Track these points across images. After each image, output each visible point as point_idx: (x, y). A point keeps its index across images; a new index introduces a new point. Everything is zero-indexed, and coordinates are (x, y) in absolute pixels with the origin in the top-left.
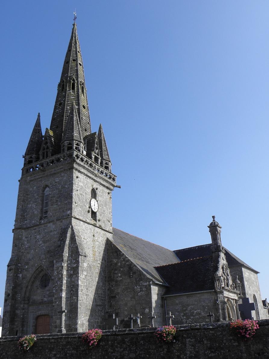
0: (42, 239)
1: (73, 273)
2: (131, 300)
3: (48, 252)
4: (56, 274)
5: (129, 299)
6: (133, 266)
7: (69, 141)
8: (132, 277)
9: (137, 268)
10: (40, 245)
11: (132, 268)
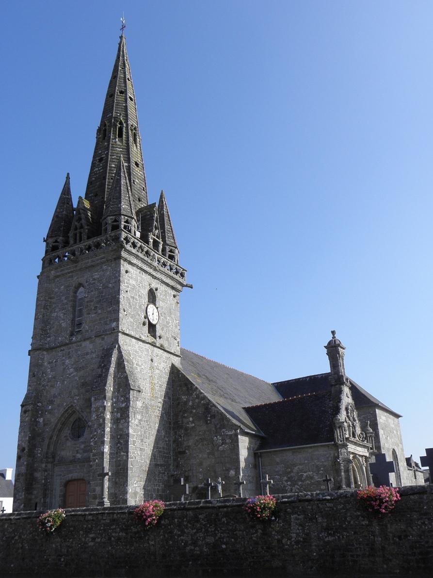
2: (208, 458)
5: (205, 456)
6: (211, 406)
8: (211, 423)
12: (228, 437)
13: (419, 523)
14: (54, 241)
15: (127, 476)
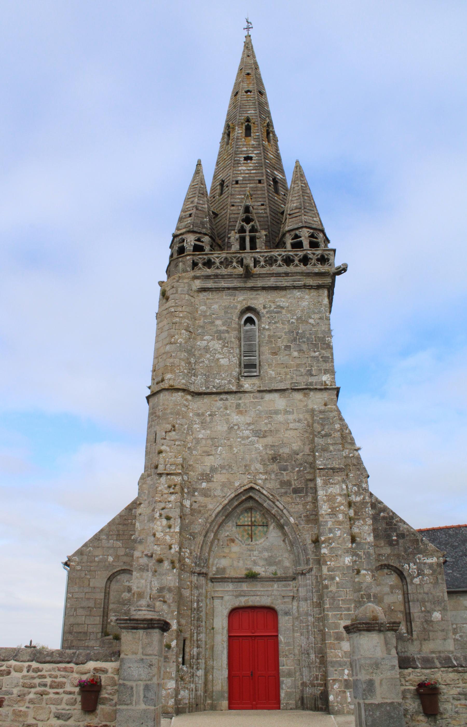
0: (249, 424)
1: (355, 514)
2: (392, 593)
3: (274, 459)
4: (325, 511)
5: (387, 589)
6: (397, 521)
7: (312, 231)
8: (398, 544)
9: (407, 526)
10: (243, 438)
11: (395, 525)
12: (427, 567)
13: (370, 708)
14: (197, 238)
15: (65, 614)
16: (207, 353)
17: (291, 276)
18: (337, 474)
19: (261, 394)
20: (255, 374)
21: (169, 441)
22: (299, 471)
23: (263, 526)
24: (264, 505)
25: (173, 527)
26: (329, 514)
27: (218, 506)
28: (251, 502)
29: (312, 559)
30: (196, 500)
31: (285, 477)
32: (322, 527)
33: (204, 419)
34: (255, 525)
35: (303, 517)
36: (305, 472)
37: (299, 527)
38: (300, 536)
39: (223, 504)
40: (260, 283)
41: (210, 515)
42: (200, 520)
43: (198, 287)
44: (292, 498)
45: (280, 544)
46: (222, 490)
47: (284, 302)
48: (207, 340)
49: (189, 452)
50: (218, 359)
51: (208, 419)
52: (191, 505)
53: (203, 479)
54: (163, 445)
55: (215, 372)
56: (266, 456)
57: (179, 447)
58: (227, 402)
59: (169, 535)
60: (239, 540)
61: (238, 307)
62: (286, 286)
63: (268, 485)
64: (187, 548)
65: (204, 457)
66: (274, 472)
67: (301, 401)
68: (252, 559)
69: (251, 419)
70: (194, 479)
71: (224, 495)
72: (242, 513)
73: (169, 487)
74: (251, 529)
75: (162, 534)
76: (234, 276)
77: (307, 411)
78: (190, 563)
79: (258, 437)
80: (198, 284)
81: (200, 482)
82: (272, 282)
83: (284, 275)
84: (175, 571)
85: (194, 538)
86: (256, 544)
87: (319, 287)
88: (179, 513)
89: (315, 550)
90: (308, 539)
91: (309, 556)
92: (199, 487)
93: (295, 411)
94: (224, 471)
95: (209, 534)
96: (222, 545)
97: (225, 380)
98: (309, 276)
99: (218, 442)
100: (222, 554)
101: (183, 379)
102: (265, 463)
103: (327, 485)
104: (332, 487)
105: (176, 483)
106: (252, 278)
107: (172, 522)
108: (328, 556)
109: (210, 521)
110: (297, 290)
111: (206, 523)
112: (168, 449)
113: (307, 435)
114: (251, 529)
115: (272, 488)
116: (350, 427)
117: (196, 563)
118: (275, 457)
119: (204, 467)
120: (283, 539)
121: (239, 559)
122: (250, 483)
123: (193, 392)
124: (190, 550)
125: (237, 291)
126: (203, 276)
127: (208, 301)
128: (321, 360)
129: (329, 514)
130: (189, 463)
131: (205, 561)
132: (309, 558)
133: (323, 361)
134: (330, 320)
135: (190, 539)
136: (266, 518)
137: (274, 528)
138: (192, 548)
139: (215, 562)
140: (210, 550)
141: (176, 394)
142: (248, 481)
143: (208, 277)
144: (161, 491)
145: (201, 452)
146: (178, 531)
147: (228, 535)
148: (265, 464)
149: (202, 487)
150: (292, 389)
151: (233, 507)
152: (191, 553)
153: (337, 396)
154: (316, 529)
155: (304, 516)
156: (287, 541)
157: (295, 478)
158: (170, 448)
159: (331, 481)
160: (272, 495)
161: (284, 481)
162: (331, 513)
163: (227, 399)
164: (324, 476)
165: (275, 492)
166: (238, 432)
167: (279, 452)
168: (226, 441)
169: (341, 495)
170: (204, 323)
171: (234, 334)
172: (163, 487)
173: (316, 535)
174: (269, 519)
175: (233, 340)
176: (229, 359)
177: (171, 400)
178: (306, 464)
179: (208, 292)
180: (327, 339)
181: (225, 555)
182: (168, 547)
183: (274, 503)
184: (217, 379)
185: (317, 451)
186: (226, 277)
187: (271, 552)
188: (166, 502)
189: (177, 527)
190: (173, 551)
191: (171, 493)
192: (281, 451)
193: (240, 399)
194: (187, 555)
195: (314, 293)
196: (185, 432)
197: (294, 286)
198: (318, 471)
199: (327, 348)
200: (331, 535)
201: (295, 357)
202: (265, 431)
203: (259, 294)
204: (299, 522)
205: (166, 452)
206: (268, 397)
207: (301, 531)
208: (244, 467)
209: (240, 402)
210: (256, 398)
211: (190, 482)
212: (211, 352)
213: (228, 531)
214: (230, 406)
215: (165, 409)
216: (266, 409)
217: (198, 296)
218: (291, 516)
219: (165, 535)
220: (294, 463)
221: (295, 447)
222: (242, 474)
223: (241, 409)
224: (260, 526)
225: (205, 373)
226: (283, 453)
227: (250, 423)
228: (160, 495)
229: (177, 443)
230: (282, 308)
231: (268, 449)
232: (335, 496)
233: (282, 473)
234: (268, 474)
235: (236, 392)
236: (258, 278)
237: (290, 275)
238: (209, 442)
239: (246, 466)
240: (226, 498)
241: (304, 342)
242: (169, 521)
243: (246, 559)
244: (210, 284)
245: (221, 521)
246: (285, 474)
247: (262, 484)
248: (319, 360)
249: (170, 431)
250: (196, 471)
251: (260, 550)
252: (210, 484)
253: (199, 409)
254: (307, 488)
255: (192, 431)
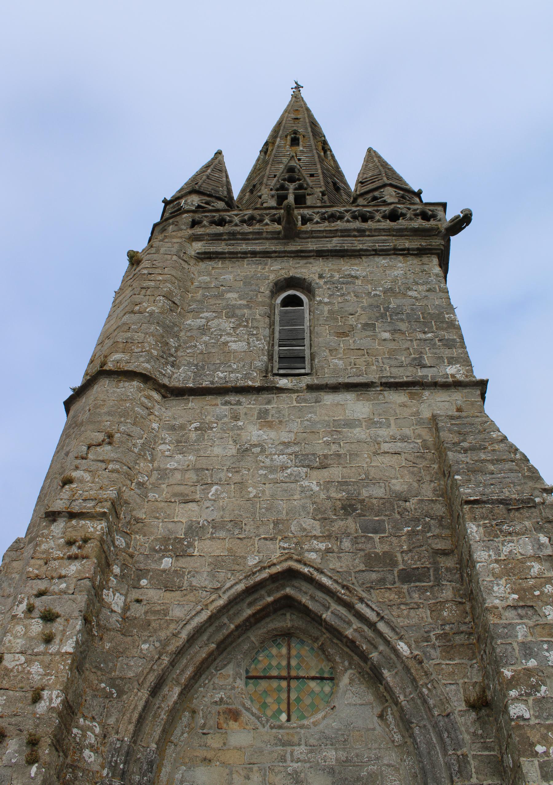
0: (286, 444)
4: (502, 599)
10: (272, 469)
16: (204, 334)
17: (369, 236)
18: (517, 514)
19: (314, 395)
20: (302, 371)
21: (92, 463)
22: (411, 534)
23: (322, 679)
24: (324, 616)
25: (57, 640)
26: (515, 608)
27: (198, 613)
28: (288, 616)
29: (474, 757)
30: (140, 598)
31: (378, 545)
32: (499, 642)
33: (183, 436)
34: (297, 678)
35: (433, 638)
36: (429, 534)
37: (426, 665)
38: (429, 689)
39: (212, 607)
40: (312, 246)
41: (175, 635)
42: (145, 647)
43: (197, 251)
44: (399, 593)
45: (371, 726)
46: (212, 575)
47: (358, 270)
48: (207, 318)
49: (139, 492)
50: (226, 343)
51: (193, 436)
52: (126, 608)
53: (166, 550)
54: (77, 468)
55: (218, 362)
56: (329, 504)
57: (115, 475)
58: (240, 407)
59: (41, 662)
60: (253, 714)
61: (270, 277)
62: (361, 250)
63: (334, 564)
64: (93, 718)
65: (173, 505)
66: (348, 535)
67: (404, 405)
68: (290, 770)
69: (292, 436)
70: (142, 551)
71: (217, 585)
72: (263, 645)
73: (70, 543)
74: (289, 686)
75: (23, 659)
76: (264, 235)
77: (420, 422)
78: (96, 768)
79: (308, 466)
80: (198, 247)
81: (157, 556)
82: (334, 243)
83: (356, 233)
84: (34, 769)
85: (121, 693)
86: (302, 727)
87: (421, 252)
88: (83, 604)
89: (480, 732)
90: (454, 699)
91: (465, 750)
92: (153, 566)
93: (392, 422)
94: (222, 534)
95: (165, 690)
96: (203, 726)
97: (238, 372)
98: (401, 236)
99: (212, 476)
100: (202, 753)
101: (148, 362)
102: (326, 516)
103: (497, 536)
104: (509, 542)
105: (88, 535)
106: (297, 239)
107: (57, 626)
108: (533, 727)
109: (172, 648)
110: (381, 258)
111: (161, 654)
112: (87, 477)
113: (423, 464)
114: (289, 686)
115: (345, 569)
116: (522, 449)
117: (113, 768)
118: (351, 506)
119: (170, 526)
120: (378, 710)
121: (251, 770)
122: (286, 560)
123: (164, 386)
124: (103, 726)
125: (269, 260)
126: (208, 235)
127: (213, 271)
128: (439, 344)
129: (515, 608)
130: (134, 513)
131: (145, 767)
132: (465, 756)
133: (444, 345)
134: (448, 292)
135: (109, 696)
136: (329, 658)
137: (351, 680)
138: (111, 721)
139: (178, 776)
140: (167, 732)
141: (127, 384)
142: (282, 555)
143: (217, 237)
144: (46, 552)
145: (169, 496)
146: (71, 650)
147: (221, 699)
148: (326, 519)
149: (162, 567)
150: (382, 384)
151: (239, 620)
152: (105, 736)
153: (483, 398)
154: (475, 671)
155: (438, 637)
156: (390, 718)
157: (405, 547)
158: (93, 476)
159: (505, 527)
160: (343, 587)
161: (376, 554)
162: (521, 604)
163: (239, 403)
164: (484, 518)
165: (354, 581)
166: (260, 458)
167: (359, 494)
168: (230, 475)
169: (538, 559)
170: (203, 296)
171: (259, 311)
172: (52, 544)
173: (477, 688)
174: (338, 659)
175: (258, 317)
176: (249, 343)
177: (114, 392)
178: (427, 519)
179: (217, 260)
180: (446, 316)
181: (209, 755)
182: (29, 695)
183: (349, 606)
184: (220, 371)
185: (458, 473)
186: (251, 237)
187: (344, 749)
188: (52, 578)
189: (70, 641)
190: (42, 707)
191: (70, 558)
192: (365, 493)
193: (269, 402)
194: (91, 739)
195: (413, 262)
196: (136, 450)
197: (375, 250)
198: (466, 507)
199: (449, 327)
200: (532, 663)
201: (385, 340)
202: (325, 456)
203: (310, 263)
204: (425, 653)
205: (81, 481)
206: (329, 399)
207: (433, 676)
208: (272, 526)
209: (269, 407)
210: (305, 401)
211: (132, 556)
212: (212, 333)
213: (222, 688)
214: (246, 414)
215: (96, 407)
216: (327, 418)
217: (195, 264)
218: (401, 638)
219: (29, 662)
220: (399, 517)
221: (398, 485)
222: (265, 539)
223: (270, 419)
224: (313, 678)
225: (195, 362)
226: (370, 497)
227: (289, 442)
228: (41, 562)
229: (111, 466)
230: (357, 278)
231: (333, 489)
232: (522, 562)
233: (371, 538)
234: (333, 540)
235: (259, 390)
236: (309, 240)
237: (367, 233)
238: (192, 476)
239: (276, 523)
240: (220, 593)
241: (402, 320)
242: (49, 625)
243: (271, 769)
244: (221, 247)
245: (204, 655)
246: (377, 539)
247: (319, 560)
248: (435, 344)
249: (99, 445)
250: (152, 533)
251: (312, 741)
252: (182, 562)
253: (175, 418)
254: (437, 570)
255: (152, 454)
